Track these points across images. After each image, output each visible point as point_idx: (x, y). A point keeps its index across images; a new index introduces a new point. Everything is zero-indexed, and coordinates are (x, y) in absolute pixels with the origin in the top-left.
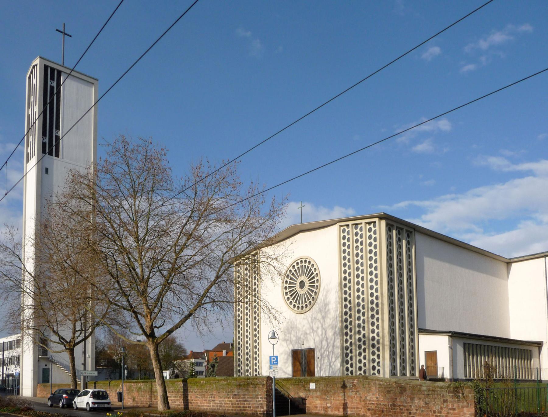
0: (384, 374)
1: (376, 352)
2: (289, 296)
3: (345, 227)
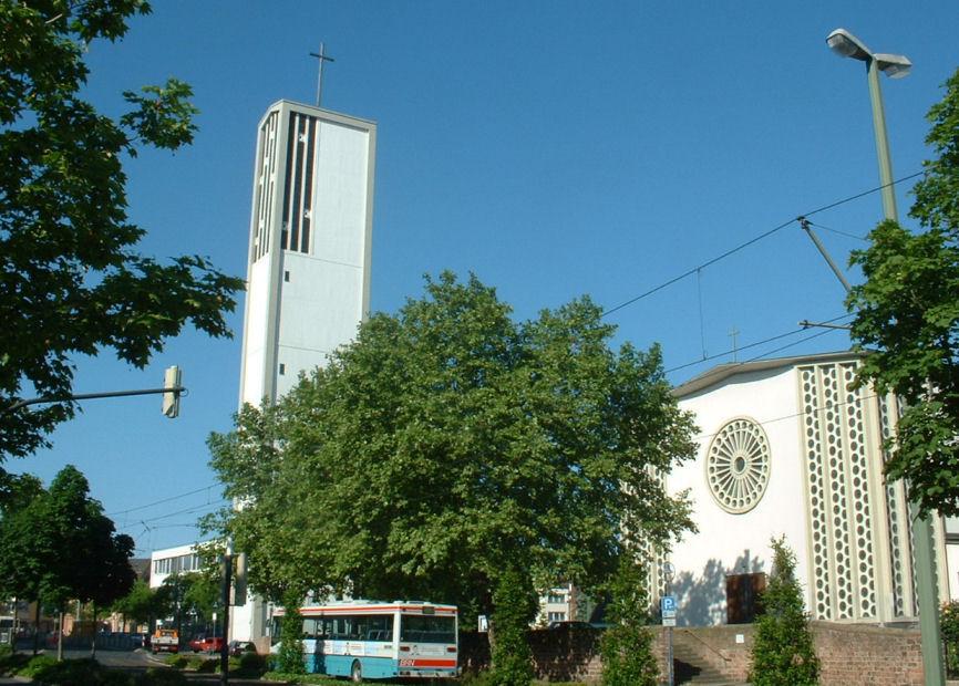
0: (882, 616)
1: (862, 491)
2: (715, 474)
3: (809, 372)
